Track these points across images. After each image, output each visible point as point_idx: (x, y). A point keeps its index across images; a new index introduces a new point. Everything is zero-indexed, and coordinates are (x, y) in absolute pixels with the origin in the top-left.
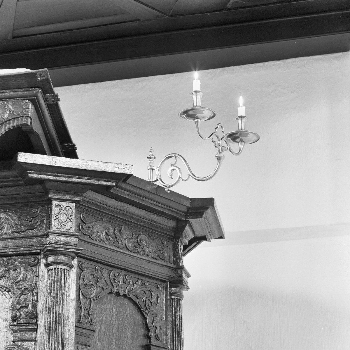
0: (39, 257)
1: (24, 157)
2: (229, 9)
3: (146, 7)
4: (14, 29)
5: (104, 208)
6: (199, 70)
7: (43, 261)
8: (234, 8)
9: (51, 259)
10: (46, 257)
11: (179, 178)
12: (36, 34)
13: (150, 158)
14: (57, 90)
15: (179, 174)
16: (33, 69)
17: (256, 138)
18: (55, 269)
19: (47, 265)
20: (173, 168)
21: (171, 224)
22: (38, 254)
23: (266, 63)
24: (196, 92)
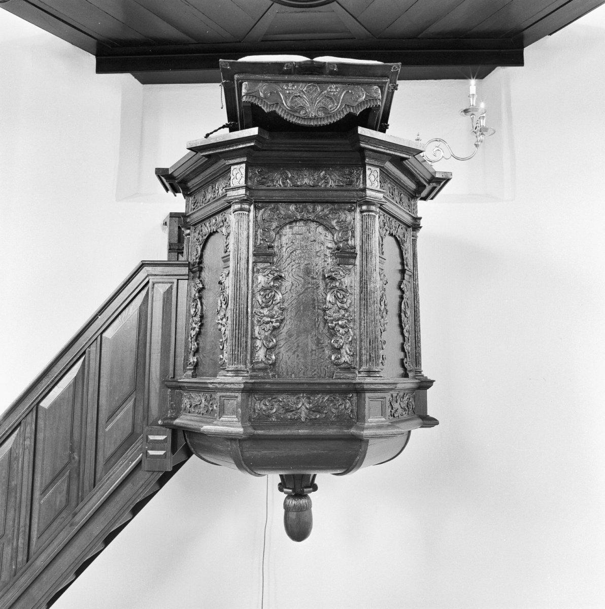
0: (355, 205)
1: (362, 130)
2: (419, 39)
3: (364, 29)
4: (265, 35)
5: (390, 174)
6: (476, 78)
7: (358, 210)
8: (423, 39)
9: (364, 208)
10: (360, 205)
11: (443, 157)
12: (284, 40)
13: (418, 140)
14: (398, 82)
15: (442, 154)
16: (385, 62)
17: (493, 132)
18: (369, 215)
19: (362, 212)
20: (437, 149)
21: (412, 186)
22: (354, 203)
23: (427, 81)
24: (473, 95)
